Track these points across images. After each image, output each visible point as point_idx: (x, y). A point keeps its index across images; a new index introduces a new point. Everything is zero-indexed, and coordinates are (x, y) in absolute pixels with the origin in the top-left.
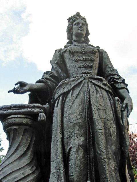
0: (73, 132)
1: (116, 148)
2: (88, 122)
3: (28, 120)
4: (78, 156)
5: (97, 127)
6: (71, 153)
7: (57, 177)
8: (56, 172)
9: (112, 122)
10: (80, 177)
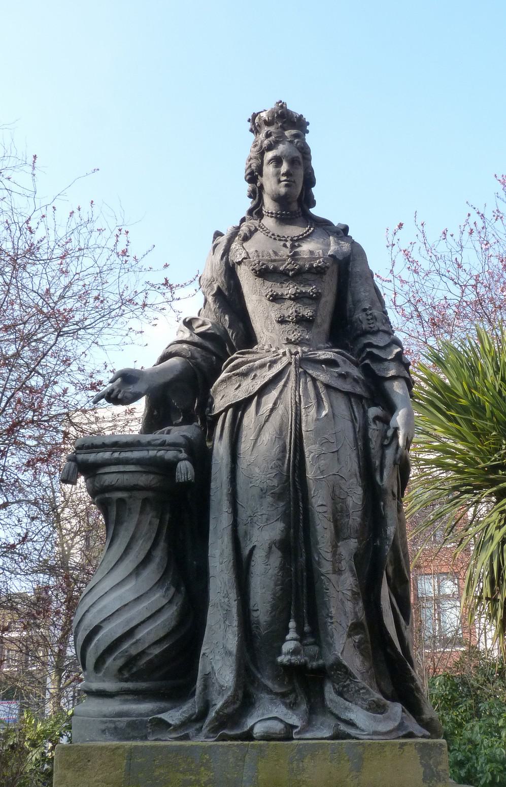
0: (259, 510)
1: (360, 544)
2: (294, 485)
3: (151, 478)
5: (313, 500)
7: (224, 614)
8: (220, 603)
9: (354, 480)
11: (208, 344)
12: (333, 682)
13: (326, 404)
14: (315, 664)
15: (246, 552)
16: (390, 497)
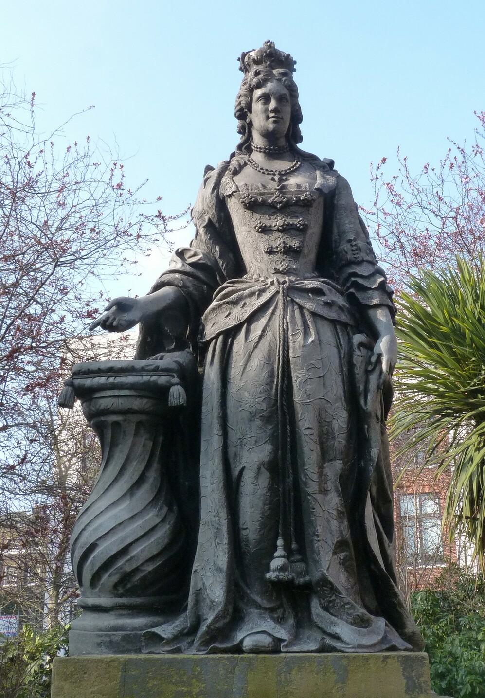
3: (145, 402)
4: (257, 487)
5: (300, 423)
6: (242, 479)
7: (214, 533)
9: (339, 404)
10: (262, 532)
11: (199, 274)
12: (319, 597)
13: (312, 331)
14: (302, 580)
15: (236, 473)
16: (374, 421)
